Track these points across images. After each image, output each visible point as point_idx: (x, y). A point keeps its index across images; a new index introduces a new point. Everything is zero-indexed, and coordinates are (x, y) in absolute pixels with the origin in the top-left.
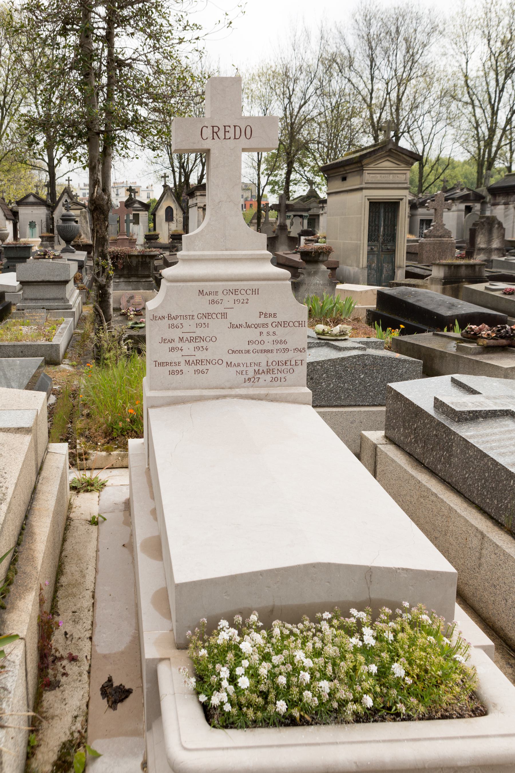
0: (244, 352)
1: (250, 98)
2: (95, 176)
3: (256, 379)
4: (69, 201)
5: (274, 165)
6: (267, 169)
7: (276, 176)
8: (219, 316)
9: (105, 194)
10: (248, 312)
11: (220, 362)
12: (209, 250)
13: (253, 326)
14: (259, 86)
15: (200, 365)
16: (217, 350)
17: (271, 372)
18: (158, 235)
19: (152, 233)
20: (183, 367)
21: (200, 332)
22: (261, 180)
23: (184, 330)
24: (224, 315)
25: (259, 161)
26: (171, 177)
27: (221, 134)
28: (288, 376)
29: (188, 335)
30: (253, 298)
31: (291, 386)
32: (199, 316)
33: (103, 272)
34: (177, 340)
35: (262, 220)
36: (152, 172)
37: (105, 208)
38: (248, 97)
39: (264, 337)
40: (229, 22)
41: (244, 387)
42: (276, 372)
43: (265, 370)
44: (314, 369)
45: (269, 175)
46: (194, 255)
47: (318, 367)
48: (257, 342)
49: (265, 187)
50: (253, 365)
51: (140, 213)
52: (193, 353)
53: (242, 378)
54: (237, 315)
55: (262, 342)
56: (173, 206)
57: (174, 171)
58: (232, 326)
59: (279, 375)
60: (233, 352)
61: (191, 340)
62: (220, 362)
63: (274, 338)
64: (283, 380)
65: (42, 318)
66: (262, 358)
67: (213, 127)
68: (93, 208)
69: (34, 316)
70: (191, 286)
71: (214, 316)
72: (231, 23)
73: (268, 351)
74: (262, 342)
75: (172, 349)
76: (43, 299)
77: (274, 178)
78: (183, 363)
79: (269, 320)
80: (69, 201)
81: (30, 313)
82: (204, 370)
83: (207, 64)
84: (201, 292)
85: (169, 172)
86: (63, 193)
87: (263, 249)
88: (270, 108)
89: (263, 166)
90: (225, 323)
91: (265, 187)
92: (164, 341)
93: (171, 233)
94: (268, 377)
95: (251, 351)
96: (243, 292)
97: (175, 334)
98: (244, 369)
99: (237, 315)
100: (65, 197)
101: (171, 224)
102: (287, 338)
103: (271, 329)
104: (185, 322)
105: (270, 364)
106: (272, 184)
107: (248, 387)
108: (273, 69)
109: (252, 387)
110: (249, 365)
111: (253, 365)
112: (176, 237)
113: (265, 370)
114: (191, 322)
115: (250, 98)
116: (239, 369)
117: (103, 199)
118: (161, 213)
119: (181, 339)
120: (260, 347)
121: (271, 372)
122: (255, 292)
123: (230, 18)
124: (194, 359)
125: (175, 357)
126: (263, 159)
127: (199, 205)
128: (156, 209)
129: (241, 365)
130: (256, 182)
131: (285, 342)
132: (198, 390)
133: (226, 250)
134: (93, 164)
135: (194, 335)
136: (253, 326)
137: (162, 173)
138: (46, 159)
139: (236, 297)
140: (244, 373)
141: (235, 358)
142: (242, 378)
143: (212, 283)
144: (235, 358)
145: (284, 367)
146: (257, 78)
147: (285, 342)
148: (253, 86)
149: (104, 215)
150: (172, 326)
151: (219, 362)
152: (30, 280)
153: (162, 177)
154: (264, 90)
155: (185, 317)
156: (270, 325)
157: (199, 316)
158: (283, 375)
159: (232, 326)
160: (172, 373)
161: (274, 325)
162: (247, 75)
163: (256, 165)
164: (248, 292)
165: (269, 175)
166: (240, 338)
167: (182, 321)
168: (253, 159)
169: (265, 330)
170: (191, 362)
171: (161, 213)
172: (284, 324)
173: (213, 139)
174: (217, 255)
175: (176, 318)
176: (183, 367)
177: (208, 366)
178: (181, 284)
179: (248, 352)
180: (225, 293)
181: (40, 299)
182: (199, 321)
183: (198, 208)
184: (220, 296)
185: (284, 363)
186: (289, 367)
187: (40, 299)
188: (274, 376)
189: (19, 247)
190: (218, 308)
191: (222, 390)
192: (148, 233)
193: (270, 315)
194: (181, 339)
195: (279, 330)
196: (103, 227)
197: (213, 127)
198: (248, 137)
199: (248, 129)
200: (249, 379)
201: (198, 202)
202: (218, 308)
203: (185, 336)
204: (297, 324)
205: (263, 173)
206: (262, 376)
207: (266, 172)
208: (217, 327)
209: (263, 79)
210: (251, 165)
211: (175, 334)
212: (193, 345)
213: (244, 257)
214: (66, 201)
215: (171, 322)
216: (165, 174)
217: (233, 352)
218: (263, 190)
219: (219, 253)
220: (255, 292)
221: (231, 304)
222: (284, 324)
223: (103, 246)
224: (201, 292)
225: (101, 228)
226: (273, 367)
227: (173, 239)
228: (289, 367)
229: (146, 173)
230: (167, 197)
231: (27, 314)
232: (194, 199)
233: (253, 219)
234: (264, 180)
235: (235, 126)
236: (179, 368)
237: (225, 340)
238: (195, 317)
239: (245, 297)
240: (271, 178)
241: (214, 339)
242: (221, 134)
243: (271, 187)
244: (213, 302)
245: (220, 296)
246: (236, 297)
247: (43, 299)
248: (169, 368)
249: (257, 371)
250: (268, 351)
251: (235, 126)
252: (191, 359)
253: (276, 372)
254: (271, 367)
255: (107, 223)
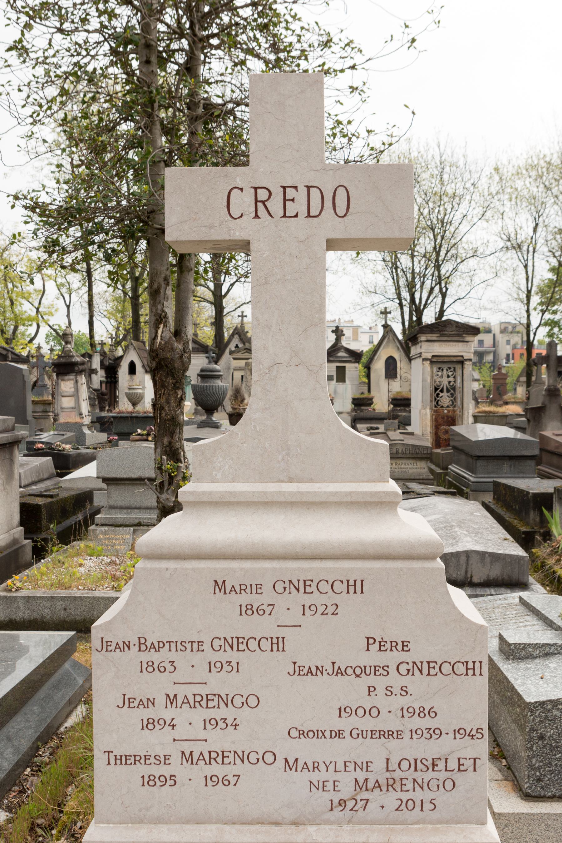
0: (327, 734)
1: (514, 200)
2: (159, 307)
3: (361, 804)
4: (240, 345)
5: (551, 298)
6: (541, 304)
7: (555, 312)
8: (266, 645)
9: (178, 341)
10: (338, 638)
11: (269, 758)
12: (247, 481)
13: (350, 671)
14: (527, 183)
15: (219, 765)
16: (257, 730)
17: (397, 786)
18: (371, 399)
19: (366, 395)
20: (176, 767)
21: (218, 683)
22: (531, 318)
23: (178, 676)
24: (278, 644)
25: (529, 292)
26: (397, 313)
27: (276, 205)
28: (441, 797)
29: (190, 691)
30: (349, 603)
31: (447, 822)
32: (216, 643)
33: (170, 484)
34: (161, 700)
35: (533, 379)
36: (369, 305)
37: (177, 364)
38: (511, 200)
39: (380, 700)
40: (410, 37)
41: (328, 822)
42: (410, 786)
43: (383, 782)
44: (546, 717)
45: (543, 312)
46: (210, 493)
47: (555, 713)
48: (360, 712)
49: (537, 328)
50: (351, 767)
51: (347, 365)
52: (202, 735)
53: (322, 799)
54: (312, 642)
55: (374, 712)
56: (396, 356)
57: (401, 305)
58: (298, 670)
59: (418, 795)
60: (301, 733)
61: (196, 702)
62: (269, 758)
63: (405, 701)
64: (428, 806)
65: (125, 543)
66: (375, 752)
67: (256, 189)
68: (154, 364)
69: (112, 539)
70: (194, 570)
71: (253, 645)
72: (413, 40)
73: (388, 734)
74: (374, 712)
75: (148, 724)
76: (139, 508)
77: (551, 317)
78: (176, 758)
79: (392, 658)
80: (240, 345)
81: (105, 533)
82: (230, 777)
83: (449, 151)
84: (220, 586)
85: (393, 306)
86: (232, 336)
87: (381, 480)
88: (545, 215)
89: (535, 300)
90: (281, 663)
91: (537, 328)
92: (128, 702)
93: (392, 396)
94: (391, 799)
95: (347, 734)
96: (324, 587)
97: (157, 686)
98: (330, 776)
99: (312, 642)
100: (236, 341)
101: (392, 382)
102: (438, 704)
103: (395, 680)
104: (182, 659)
105: (393, 765)
106: (550, 325)
107: (339, 822)
108: (548, 159)
109: (350, 821)
110: (340, 766)
111: (351, 767)
112: (399, 402)
113: (383, 782)
114: (196, 658)
115: (514, 200)
116: (315, 776)
117: (173, 349)
118: (379, 366)
119: (171, 700)
120: (368, 724)
121: (397, 786)
122: (355, 586)
123: (413, 32)
124: (205, 748)
125: (157, 742)
126: (534, 289)
127: (424, 355)
128: (371, 360)
129: (322, 767)
130: (524, 321)
131: (432, 713)
132: (214, 827)
133: (291, 480)
134: (155, 286)
135: (204, 691)
136: (350, 671)
137: (382, 307)
138: (211, 285)
139: (308, 600)
140: (329, 786)
141: (306, 750)
142: (322, 799)
143: (247, 565)
144: (306, 750)
145: (431, 774)
146: (524, 172)
147: (432, 713)
148: (519, 184)
149: (173, 377)
150: (148, 667)
151: (267, 758)
152: (119, 476)
153: (382, 313)
154: (535, 189)
155: (180, 646)
156: (392, 669)
157: (216, 643)
158: (427, 795)
159: (298, 670)
160: (149, 781)
161: (403, 669)
162: (510, 167)
163: (523, 296)
164: (338, 587)
165: (543, 312)
166: (318, 702)
167: (173, 655)
168: (519, 288)
169: (380, 683)
170: (195, 756)
171: (379, 366)
172: (429, 668)
173: (257, 216)
174: (265, 493)
175: (157, 647)
176: (176, 767)
177: (239, 768)
178: (172, 565)
179: (339, 734)
180: (279, 588)
181: (136, 508)
182: (215, 657)
183: (423, 360)
184: (267, 596)
185: (429, 763)
186: (443, 775)
187: (136, 508)
188: (405, 797)
189: (136, 417)
190: (263, 626)
191: (274, 829)
192: (358, 396)
193: (394, 645)
194: (171, 700)
195: (418, 684)
196: (172, 400)
197: (256, 189)
198: (341, 211)
199: (341, 195)
200: (342, 803)
201: (422, 351)
202: (263, 626)
203: (181, 691)
204: (460, 669)
205: (535, 309)
206: (376, 797)
207: (540, 308)
208: (260, 672)
209: (533, 173)
210: (516, 296)
211: (157, 686)
212: (199, 715)
213: (331, 499)
214: (237, 346)
215: (145, 657)
216: (386, 308)
217: (301, 733)
218: (535, 334)
219: (272, 487)
220: (355, 586)
221: (295, 616)
222: (429, 668)
223: (172, 434)
224: (220, 586)
225: (168, 402)
226: (403, 775)
227: (395, 405)
228: (443, 775)
229: (359, 307)
230: (388, 342)
231: (101, 536)
232: (418, 346)
233: (521, 375)
234: (535, 320)
235: (308, 188)
236: (166, 771)
237: (282, 704)
238: (206, 646)
239: (330, 599)
240: (547, 316)
241: (252, 701)
242: (276, 205)
243: (548, 329)
244: (249, 610)
245: (267, 596)
246: (308, 600)
247: (139, 508)
248: (146, 770)
249: (361, 782)
250: (388, 734)
251: (308, 188)
252: (197, 748)
253: (410, 786)
254: (398, 775)
255: (180, 393)
